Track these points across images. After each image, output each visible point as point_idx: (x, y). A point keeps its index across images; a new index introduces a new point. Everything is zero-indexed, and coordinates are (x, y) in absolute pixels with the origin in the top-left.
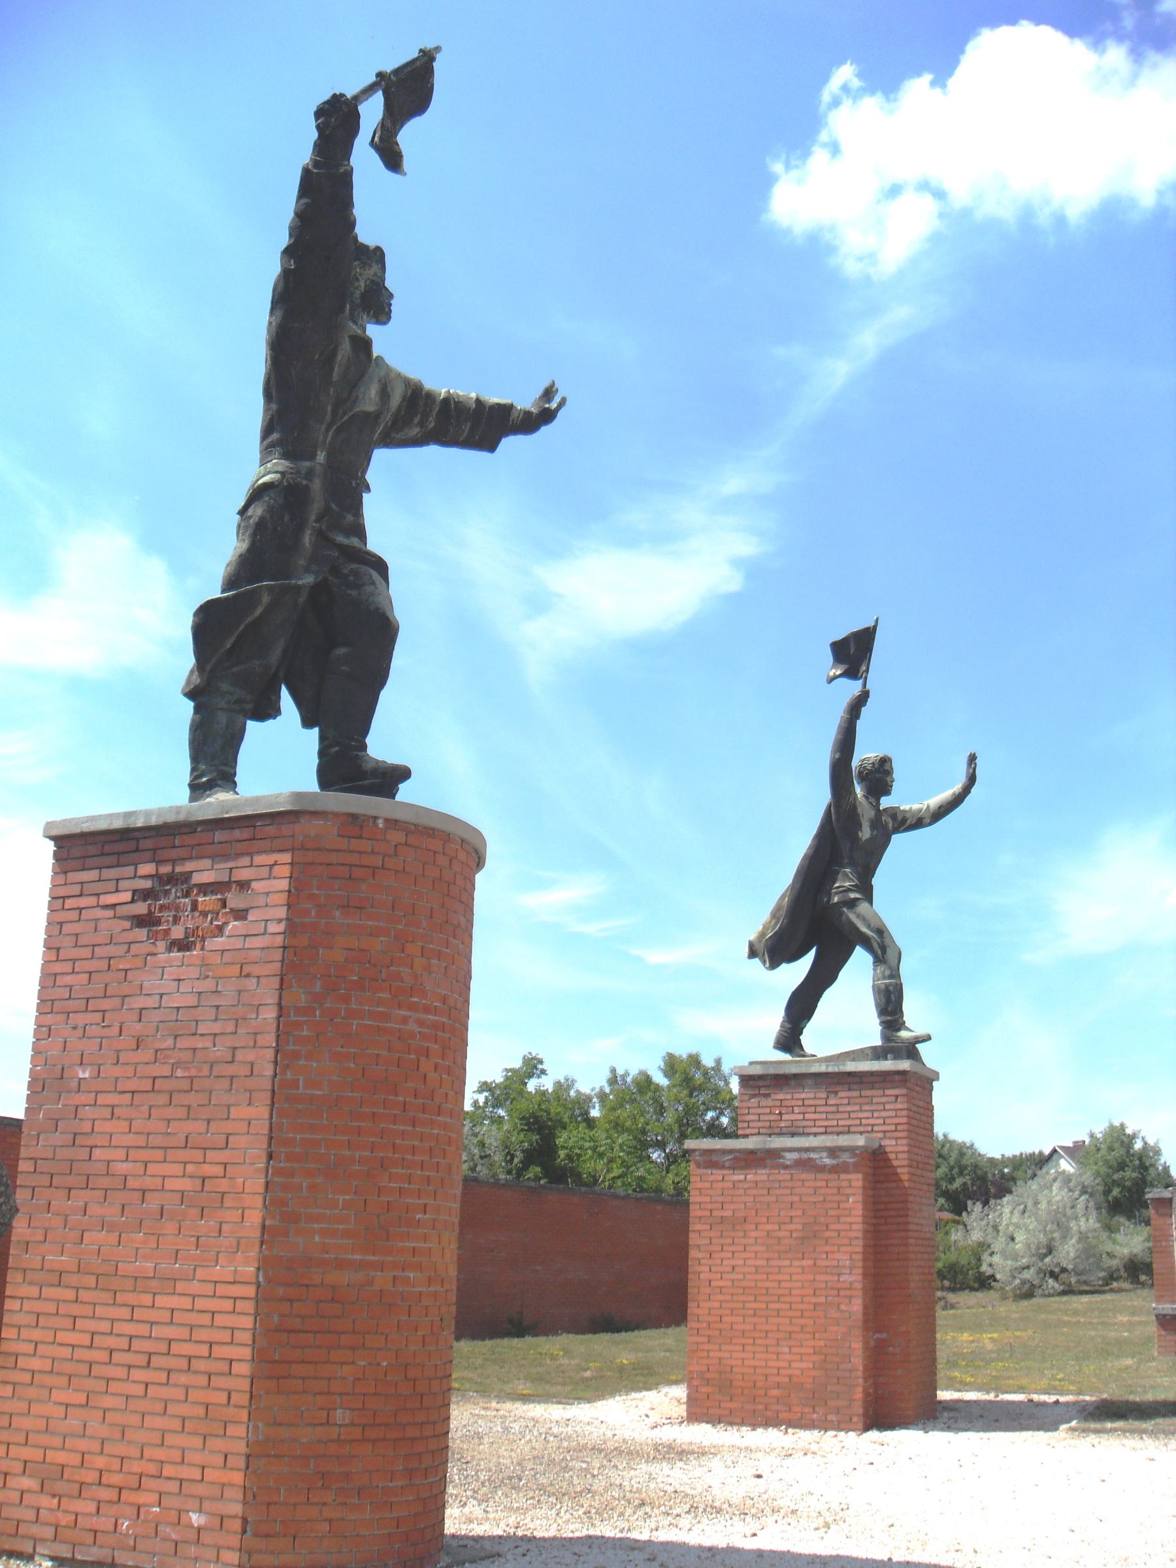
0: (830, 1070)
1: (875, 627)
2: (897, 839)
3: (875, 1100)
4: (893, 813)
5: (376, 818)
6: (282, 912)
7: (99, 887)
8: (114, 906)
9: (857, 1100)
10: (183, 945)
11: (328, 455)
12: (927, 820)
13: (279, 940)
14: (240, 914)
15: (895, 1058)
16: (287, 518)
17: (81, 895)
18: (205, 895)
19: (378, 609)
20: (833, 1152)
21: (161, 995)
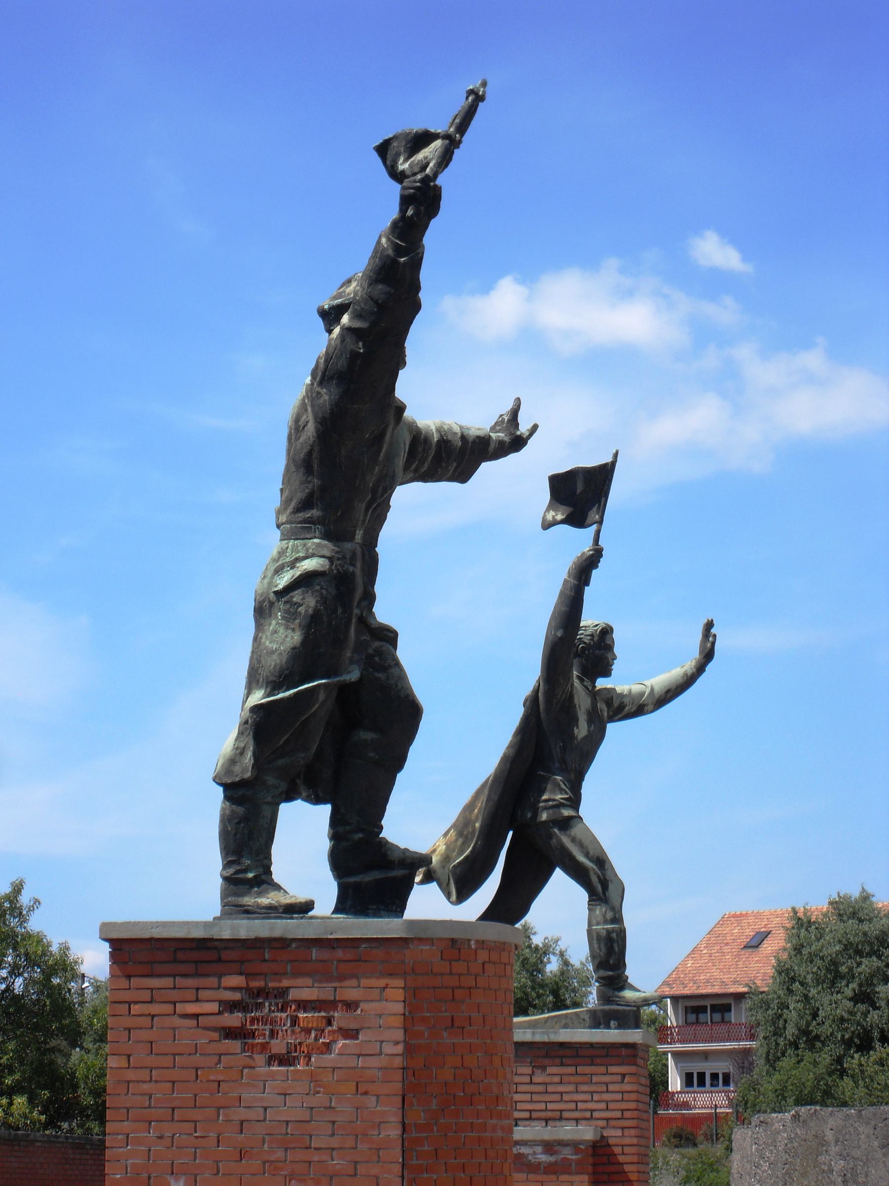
0: (538, 1038)
1: (614, 463)
2: (613, 729)
3: (595, 1079)
4: (609, 696)
5: (469, 940)
6: (399, 1035)
7: (174, 995)
8: (196, 1016)
9: (572, 1079)
10: (285, 1060)
11: (365, 534)
12: (650, 707)
13: (398, 1062)
14: (350, 1034)
15: (619, 1027)
16: (340, 611)
17: (151, 1002)
18: (305, 1012)
19: (408, 696)
20: (549, 1147)
21: (265, 1109)
